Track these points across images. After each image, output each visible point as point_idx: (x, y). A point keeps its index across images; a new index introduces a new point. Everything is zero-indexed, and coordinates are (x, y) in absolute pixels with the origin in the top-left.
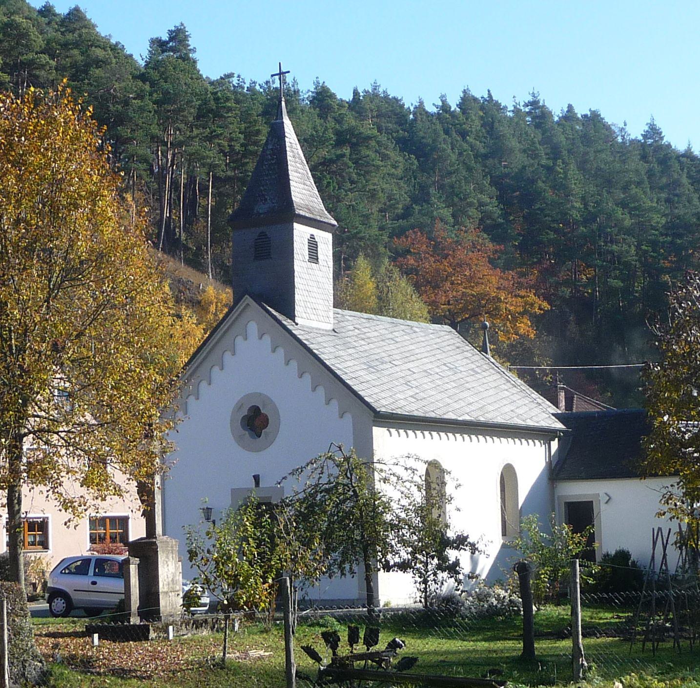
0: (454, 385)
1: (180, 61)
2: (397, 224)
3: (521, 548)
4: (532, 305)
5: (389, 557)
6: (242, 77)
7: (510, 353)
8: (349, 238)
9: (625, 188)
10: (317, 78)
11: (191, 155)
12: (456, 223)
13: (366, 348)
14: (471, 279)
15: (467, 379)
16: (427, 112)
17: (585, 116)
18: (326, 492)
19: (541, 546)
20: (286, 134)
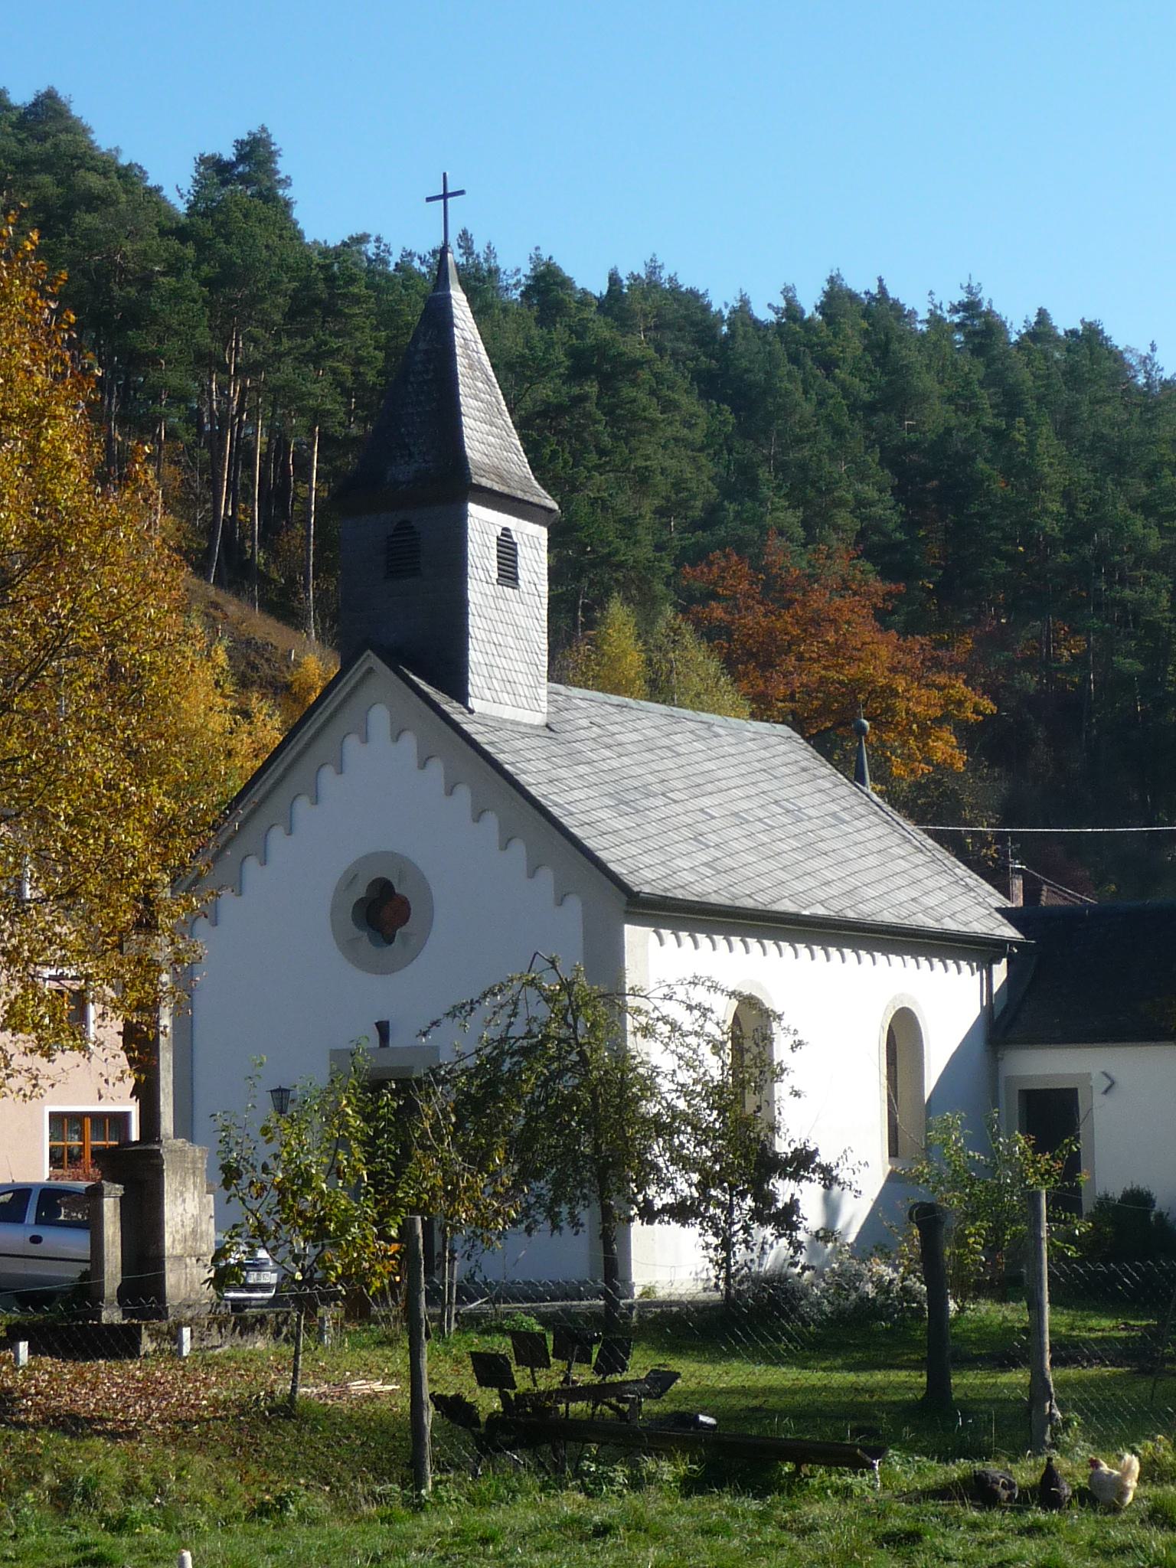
0: (795, 844)
1: (257, 201)
2: (691, 539)
3: (927, 1181)
4: (960, 704)
5: (651, 1191)
6: (385, 241)
7: (914, 800)
8: (593, 565)
9: (1151, 476)
10: (537, 248)
11: (275, 390)
12: (810, 539)
13: (615, 764)
14: (836, 650)
15: (822, 833)
16: (756, 321)
17: (1073, 333)
18: (521, 1055)
19: (970, 1178)
20: (456, 321)
